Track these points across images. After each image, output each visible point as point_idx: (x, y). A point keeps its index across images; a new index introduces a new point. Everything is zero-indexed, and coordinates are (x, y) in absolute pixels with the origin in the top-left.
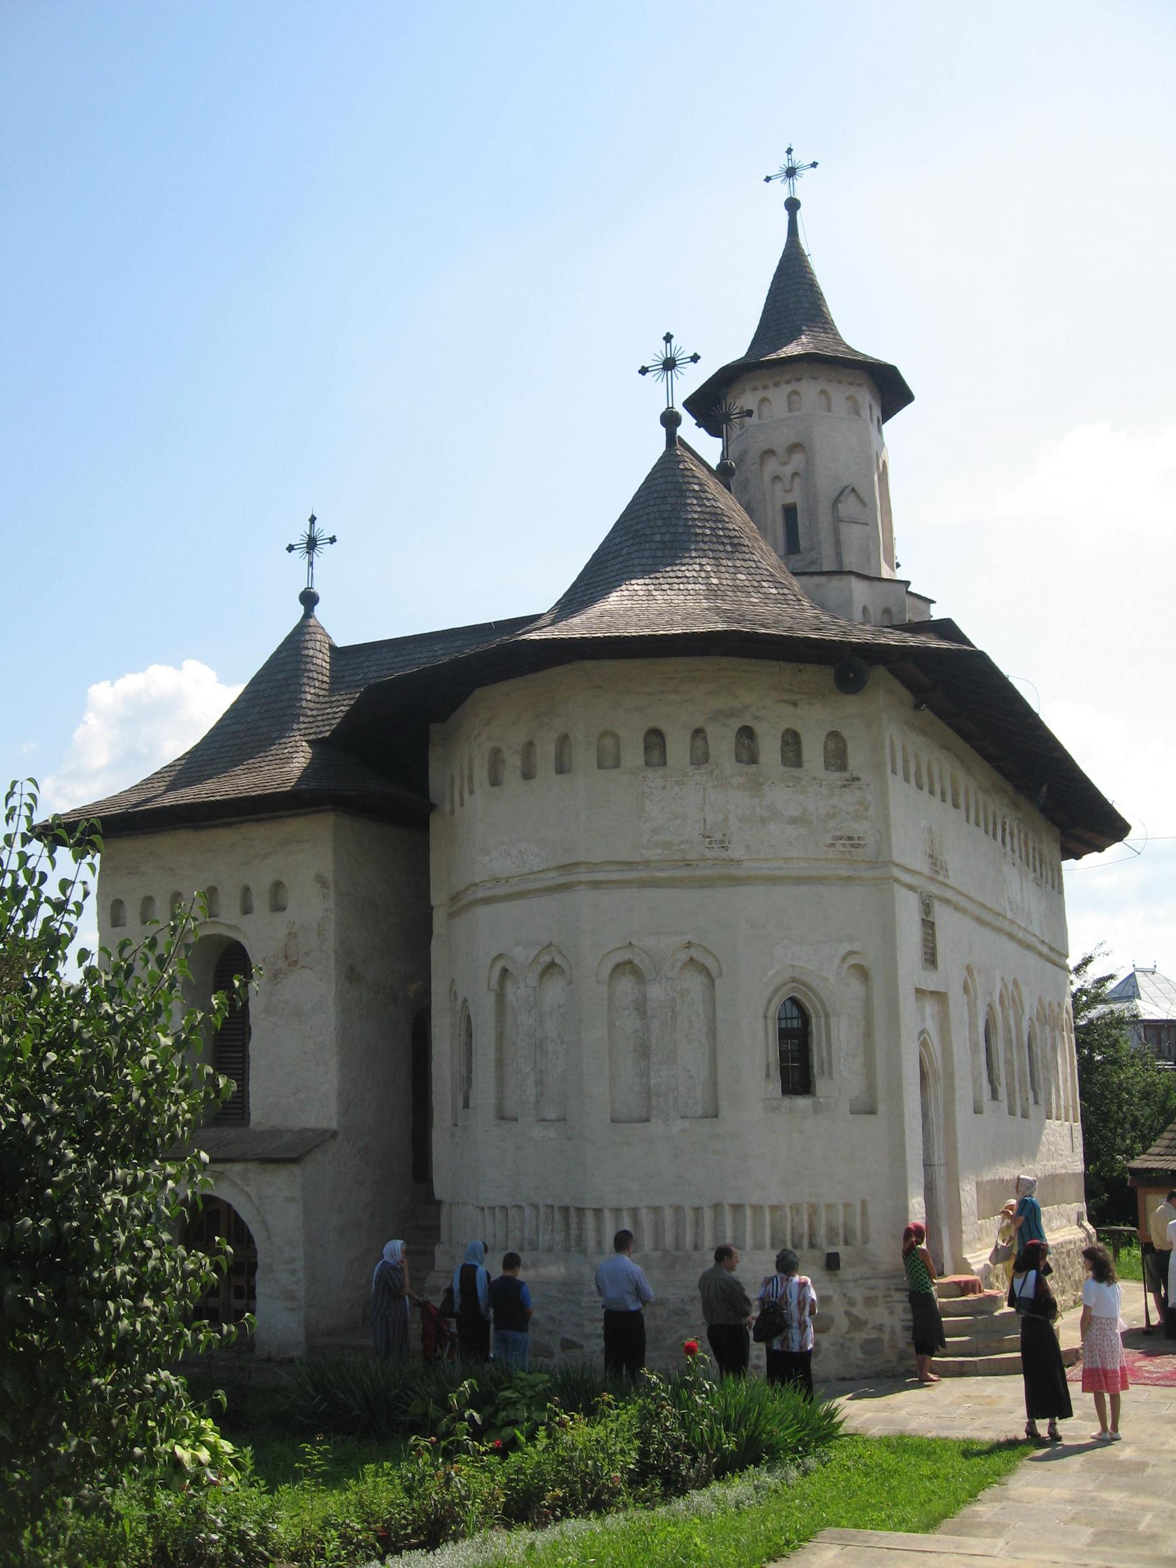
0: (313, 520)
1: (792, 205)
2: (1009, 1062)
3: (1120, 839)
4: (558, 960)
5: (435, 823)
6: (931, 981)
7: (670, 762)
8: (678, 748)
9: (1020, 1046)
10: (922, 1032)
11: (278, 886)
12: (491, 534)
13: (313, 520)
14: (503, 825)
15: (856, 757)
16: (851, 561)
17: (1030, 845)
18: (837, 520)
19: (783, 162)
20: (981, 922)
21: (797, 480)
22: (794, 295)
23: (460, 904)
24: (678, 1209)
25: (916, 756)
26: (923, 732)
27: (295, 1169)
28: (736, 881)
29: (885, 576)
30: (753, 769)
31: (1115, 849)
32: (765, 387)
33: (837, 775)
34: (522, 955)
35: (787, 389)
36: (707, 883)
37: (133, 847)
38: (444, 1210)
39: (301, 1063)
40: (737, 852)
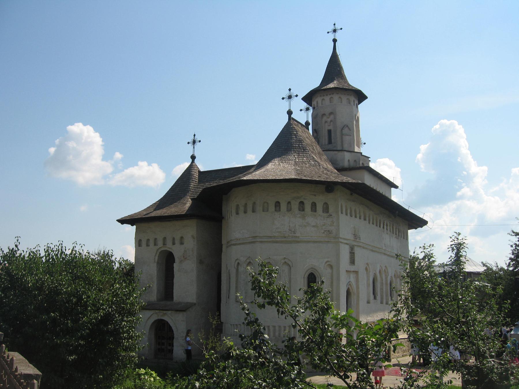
0: (195, 135)
1: (335, 41)
2: (382, 289)
3: (426, 225)
4: (251, 261)
5: (223, 221)
6: (352, 268)
7: (281, 210)
8: (284, 206)
9: (386, 284)
10: (349, 282)
11: (182, 238)
12: (239, 145)
13: (195, 135)
14: (240, 225)
15: (331, 210)
16: (346, 147)
17: (394, 227)
18: (342, 135)
19: (333, 28)
20: (372, 251)
21: (332, 123)
22: (334, 69)
23: (229, 244)
24: (280, 327)
25: (350, 208)
26: (354, 201)
27: (185, 313)
28: (298, 242)
29: (356, 151)
30: (303, 213)
31: (425, 227)
32: (324, 96)
33: (326, 214)
34: (243, 259)
35: (329, 97)
36: (291, 242)
37: (145, 225)
38: (224, 324)
39: (187, 284)
40: (298, 234)
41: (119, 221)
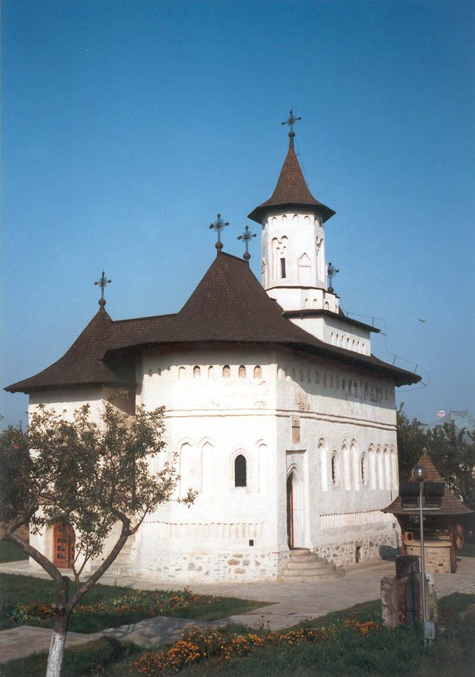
0: (103, 273)
1: (292, 135)
13: (103, 273)
41: (7, 389)
